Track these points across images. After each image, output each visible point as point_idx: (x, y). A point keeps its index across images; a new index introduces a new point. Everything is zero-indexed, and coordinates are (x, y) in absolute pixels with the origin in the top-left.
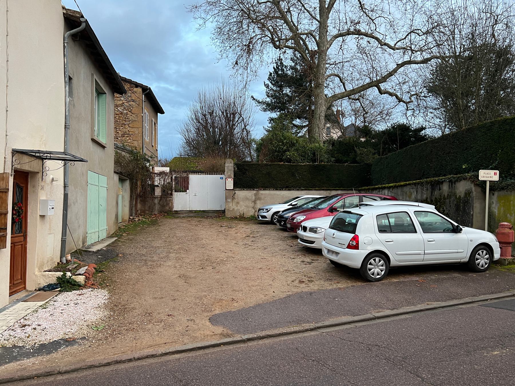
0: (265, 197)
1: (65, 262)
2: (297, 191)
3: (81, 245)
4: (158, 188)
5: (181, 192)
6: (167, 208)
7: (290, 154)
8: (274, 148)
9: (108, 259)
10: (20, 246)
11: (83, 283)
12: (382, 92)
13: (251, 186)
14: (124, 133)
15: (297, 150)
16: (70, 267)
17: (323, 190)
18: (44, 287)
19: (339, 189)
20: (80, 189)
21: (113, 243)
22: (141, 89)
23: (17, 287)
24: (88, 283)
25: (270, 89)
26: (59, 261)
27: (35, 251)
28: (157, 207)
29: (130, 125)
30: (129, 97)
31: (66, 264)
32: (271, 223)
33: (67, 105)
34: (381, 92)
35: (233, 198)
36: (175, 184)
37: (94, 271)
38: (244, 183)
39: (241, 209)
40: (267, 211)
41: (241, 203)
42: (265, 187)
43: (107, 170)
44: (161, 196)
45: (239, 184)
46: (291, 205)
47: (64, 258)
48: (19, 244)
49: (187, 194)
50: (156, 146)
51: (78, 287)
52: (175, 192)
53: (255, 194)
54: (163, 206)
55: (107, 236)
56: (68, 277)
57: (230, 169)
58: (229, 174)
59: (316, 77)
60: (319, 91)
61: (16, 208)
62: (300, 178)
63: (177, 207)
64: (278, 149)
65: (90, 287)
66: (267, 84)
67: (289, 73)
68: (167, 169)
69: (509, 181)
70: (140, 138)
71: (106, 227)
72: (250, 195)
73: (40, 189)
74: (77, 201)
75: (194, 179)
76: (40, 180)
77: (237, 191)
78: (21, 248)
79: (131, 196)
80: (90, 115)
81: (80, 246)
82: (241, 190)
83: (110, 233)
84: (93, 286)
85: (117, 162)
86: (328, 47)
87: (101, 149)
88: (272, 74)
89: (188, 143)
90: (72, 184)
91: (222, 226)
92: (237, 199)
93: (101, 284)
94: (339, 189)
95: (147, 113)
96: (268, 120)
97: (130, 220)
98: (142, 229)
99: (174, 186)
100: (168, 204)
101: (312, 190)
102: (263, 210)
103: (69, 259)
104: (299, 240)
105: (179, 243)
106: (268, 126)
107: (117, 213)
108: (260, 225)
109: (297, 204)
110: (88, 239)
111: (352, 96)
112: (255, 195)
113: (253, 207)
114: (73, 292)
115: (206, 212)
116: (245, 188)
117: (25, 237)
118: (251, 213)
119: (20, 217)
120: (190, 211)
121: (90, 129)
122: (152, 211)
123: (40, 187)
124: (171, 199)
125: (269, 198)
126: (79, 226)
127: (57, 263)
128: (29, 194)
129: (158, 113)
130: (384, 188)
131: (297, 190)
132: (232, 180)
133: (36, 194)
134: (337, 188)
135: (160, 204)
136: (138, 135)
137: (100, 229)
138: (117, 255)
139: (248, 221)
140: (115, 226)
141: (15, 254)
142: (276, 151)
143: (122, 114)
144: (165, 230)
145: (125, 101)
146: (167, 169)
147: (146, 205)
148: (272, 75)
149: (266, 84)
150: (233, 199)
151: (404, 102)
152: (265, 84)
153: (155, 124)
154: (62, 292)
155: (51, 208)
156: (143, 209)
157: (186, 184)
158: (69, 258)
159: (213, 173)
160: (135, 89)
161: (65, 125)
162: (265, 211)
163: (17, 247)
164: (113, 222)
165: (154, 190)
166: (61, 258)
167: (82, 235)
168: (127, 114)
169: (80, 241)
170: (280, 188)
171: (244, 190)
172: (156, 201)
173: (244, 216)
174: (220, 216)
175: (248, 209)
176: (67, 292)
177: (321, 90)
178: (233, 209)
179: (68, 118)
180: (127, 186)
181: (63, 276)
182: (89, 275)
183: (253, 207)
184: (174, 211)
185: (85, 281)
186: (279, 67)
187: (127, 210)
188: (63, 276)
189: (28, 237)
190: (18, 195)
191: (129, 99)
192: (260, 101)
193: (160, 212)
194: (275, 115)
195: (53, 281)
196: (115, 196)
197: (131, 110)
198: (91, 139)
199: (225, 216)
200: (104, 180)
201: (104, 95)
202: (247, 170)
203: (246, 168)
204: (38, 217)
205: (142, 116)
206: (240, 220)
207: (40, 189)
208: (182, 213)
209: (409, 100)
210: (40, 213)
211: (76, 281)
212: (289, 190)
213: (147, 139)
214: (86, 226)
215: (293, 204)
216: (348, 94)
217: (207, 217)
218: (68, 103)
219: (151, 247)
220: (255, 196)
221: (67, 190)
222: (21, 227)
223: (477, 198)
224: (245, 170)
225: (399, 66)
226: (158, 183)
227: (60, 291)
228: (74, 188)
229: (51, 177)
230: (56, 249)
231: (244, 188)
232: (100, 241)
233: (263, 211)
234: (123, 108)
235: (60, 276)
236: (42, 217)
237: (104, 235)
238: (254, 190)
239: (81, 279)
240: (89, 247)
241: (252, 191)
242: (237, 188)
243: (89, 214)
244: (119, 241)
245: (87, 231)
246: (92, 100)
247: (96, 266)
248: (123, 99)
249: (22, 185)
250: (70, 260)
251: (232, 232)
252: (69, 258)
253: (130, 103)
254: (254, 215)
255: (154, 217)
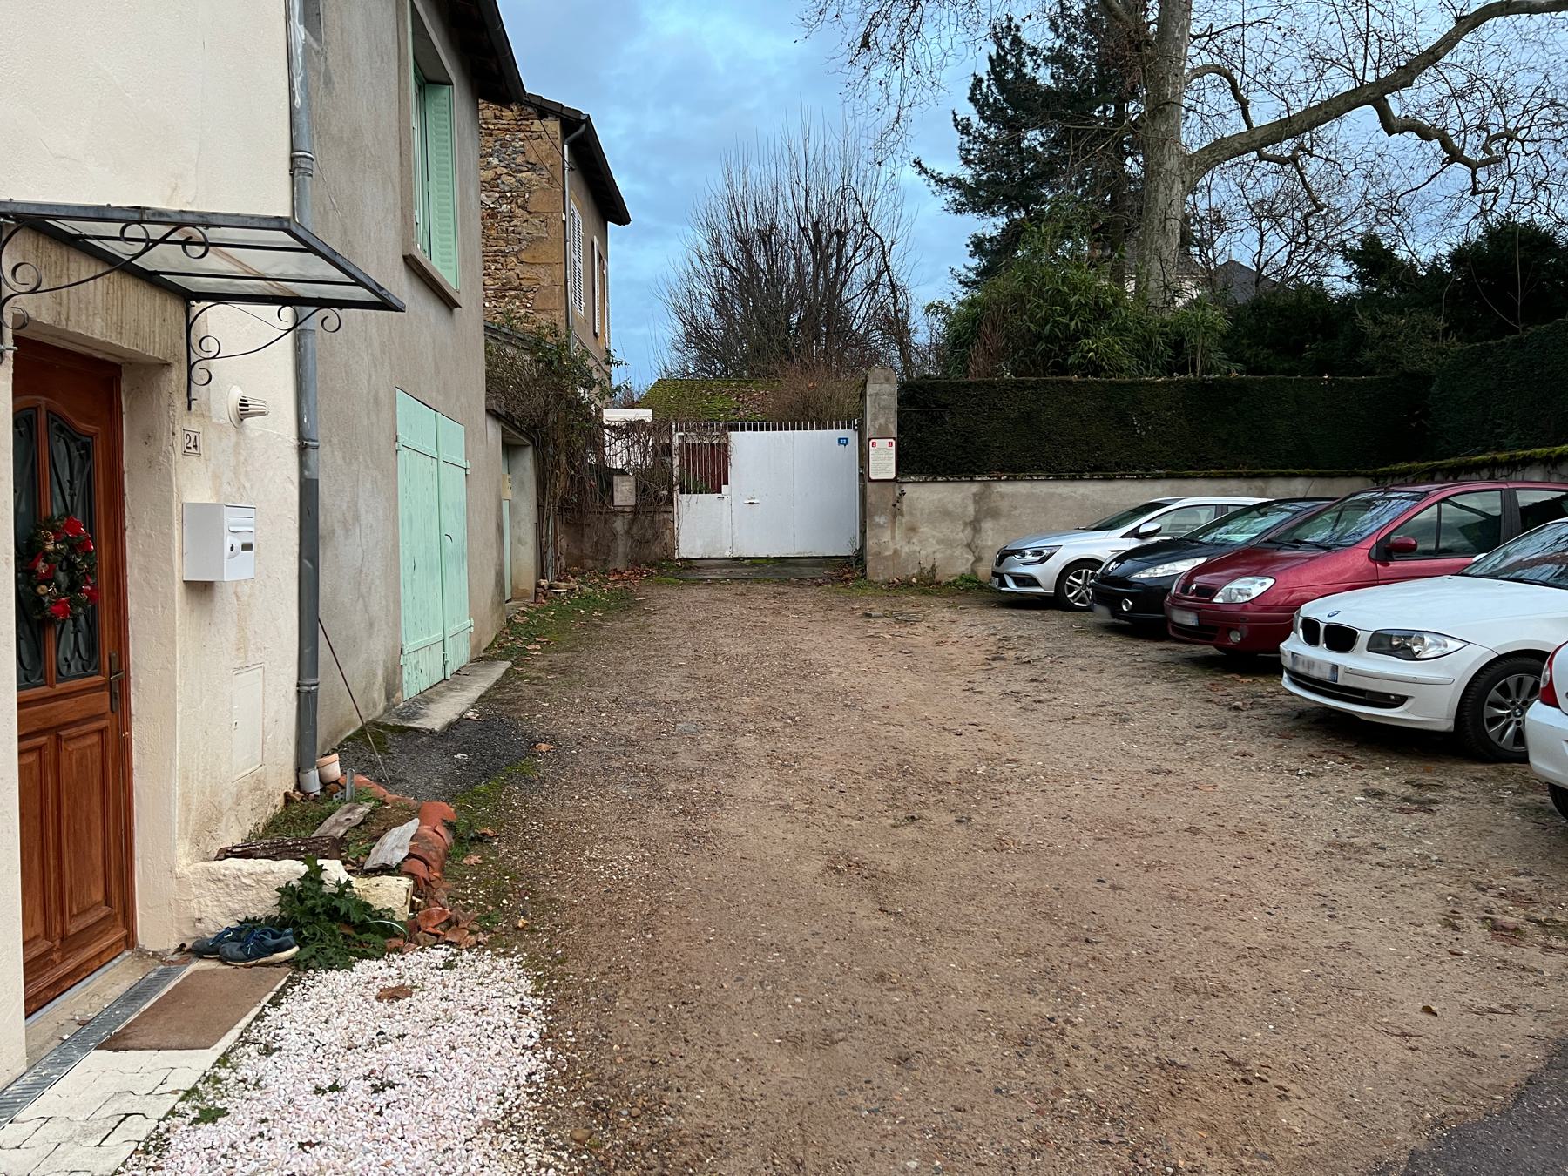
0: (1016, 508)
1: (315, 788)
2: (1136, 483)
3: (382, 705)
4: (625, 477)
5: (701, 492)
6: (657, 549)
7: (1097, 347)
8: (1032, 326)
9: (497, 769)
10: (95, 739)
11: (403, 913)
12: (1396, 124)
13: (959, 465)
14: (503, 285)
15: (1119, 331)
16: (336, 825)
17: (1238, 476)
18: (220, 938)
19: (1297, 471)
20: (367, 467)
21: (499, 685)
22: (558, 123)
23: (84, 946)
24: (429, 917)
25: (975, 137)
26: (290, 788)
27: (172, 760)
28: (622, 546)
29: (523, 256)
30: (517, 153)
31: (325, 801)
32: (1055, 602)
33: (298, 61)
34: (1390, 125)
35: (896, 512)
36: (681, 466)
37: (448, 839)
38: (934, 456)
39: (923, 553)
40: (1039, 558)
41: (924, 529)
42: (1015, 470)
43: (463, 400)
44: (636, 505)
45: (912, 463)
46: (1135, 534)
47: (314, 774)
48: (85, 728)
49: (721, 500)
50: (606, 335)
51: (378, 939)
52: (682, 492)
53: (975, 495)
54: (642, 542)
55: (471, 654)
56: (329, 888)
57: (883, 403)
58: (882, 421)
59: (1155, 81)
61: (50, 547)
62: (1147, 431)
63: (689, 546)
64: (1048, 327)
65: (437, 935)
66: (962, 120)
67: (1044, 77)
68: (646, 415)
70: (558, 303)
71: (467, 623)
72: (959, 501)
73: (179, 449)
74: (357, 518)
75: (744, 445)
76: (180, 402)
77: (909, 485)
78: (97, 751)
79: (540, 507)
80: (397, 153)
81: (375, 705)
82: (948, 481)
83: (480, 641)
84: (446, 932)
85: (494, 382)
87: (443, 311)
88: (981, 81)
89: (697, 336)
90: (335, 440)
91: (869, 616)
92: (911, 514)
93: (486, 922)
94: (1297, 471)
95: (577, 216)
96: (968, 246)
97: (539, 590)
98: (591, 626)
99: (676, 472)
100: (658, 536)
101: (1194, 477)
102: (1023, 555)
103: (333, 778)
104: (1285, 681)
105: (750, 685)
106: (965, 267)
107: (502, 565)
108: (1007, 611)
109: (1159, 529)
110: (405, 677)
111: (1268, 150)
112: (978, 499)
113: (968, 546)
114: (358, 966)
115: (790, 564)
116: (940, 475)
117: (118, 690)
118: (961, 564)
119: (81, 591)
120: (735, 559)
121: (398, 213)
122: (605, 561)
123: (179, 442)
124: (670, 516)
125: (1028, 511)
126: (371, 625)
127: (282, 796)
128: (126, 476)
129: (609, 223)
130: (1527, 462)
131: (1138, 478)
132: (890, 444)
133: (158, 467)
134: (1292, 471)
135: (632, 537)
136: (553, 290)
137: (450, 630)
138: (532, 745)
139: (954, 594)
140: (495, 617)
141: (64, 785)
142: (1039, 338)
143: (492, 216)
144: (674, 630)
145: (505, 171)
146: (646, 415)
147: (586, 539)
148: (984, 85)
149: (959, 118)
150: (894, 517)
151: (1467, 162)
152: (955, 120)
153: (600, 258)
154: (307, 968)
155: (238, 545)
156: (576, 552)
157: (719, 462)
158: (334, 768)
159: (799, 425)
160: (537, 125)
161: (292, 159)
162: (1029, 557)
163: (72, 746)
164: (489, 601)
165: (610, 485)
166: (299, 770)
167: (385, 662)
168: (511, 215)
169: (376, 687)
170: (1072, 471)
171: (935, 481)
172: (619, 525)
173: (937, 578)
174: (849, 576)
175: (949, 552)
176: (330, 967)
177: (1172, 123)
178: (896, 552)
179: (302, 119)
180: (525, 469)
181: (308, 884)
182: (427, 864)
183: (968, 546)
184: (680, 559)
185: (413, 902)
186: (1009, 57)
187: (527, 556)
188: (308, 884)
189: (133, 690)
190: (65, 476)
191: (519, 161)
193: (634, 563)
194: (992, 225)
195: (263, 904)
196: (494, 501)
197: (526, 201)
198: (405, 258)
199: (864, 577)
200: (453, 438)
201: (445, 91)
202: (945, 406)
203: (943, 398)
204: (179, 588)
205: (565, 222)
206: (925, 593)
207: (179, 449)
208: (709, 567)
209: (1481, 156)
210: (184, 569)
211: (368, 906)
212: (1107, 479)
213: (580, 310)
214: (397, 625)
215: (1142, 530)
216: (1257, 141)
217: (800, 582)
218: (300, 50)
219: (650, 704)
220: (976, 502)
221: (311, 463)
222: (93, 646)
224: (938, 406)
225: (1464, 23)
226: (625, 460)
227: (293, 962)
228: (344, 458)
229: (236, 395)
230: (274, 737)
231: (933, 473)
232: (448, 677)
233: (1023, 560)
234: (497, 195)
235: (295, 883)
236: (201, 590)
237: (460, 654)
238: (972, 481)
239: (391, 894)
240: (414, 709)
241: (966, 485)
242: (910, 474)
243: (405, 574)
244: (521, 677)
245: (403, 642)
246: (402, 89)
247: (448, 810)
248: (496, 161)
249: (85, 427)
250: (336, 782)
251: (920, 636)
252: (334, 768)
253: (520, 175)
254: (974, 572)
255: (616, 582)
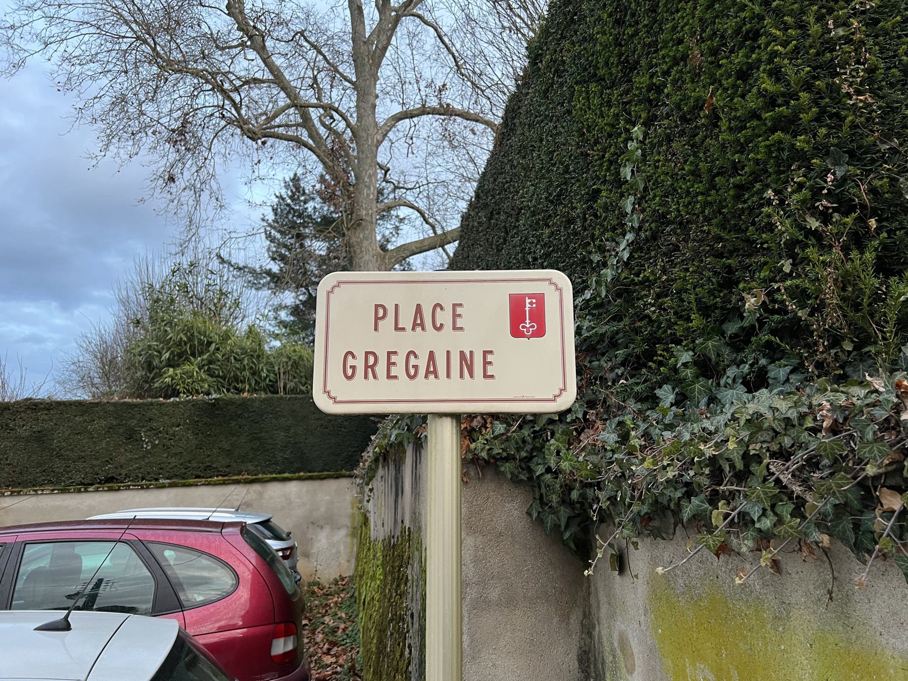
2: (142, 492)
60: (361, 236)
69: (9, 539)
86: (378, 141)
131: (142, 488)
192: (241, 266)
223: (494, 594)
